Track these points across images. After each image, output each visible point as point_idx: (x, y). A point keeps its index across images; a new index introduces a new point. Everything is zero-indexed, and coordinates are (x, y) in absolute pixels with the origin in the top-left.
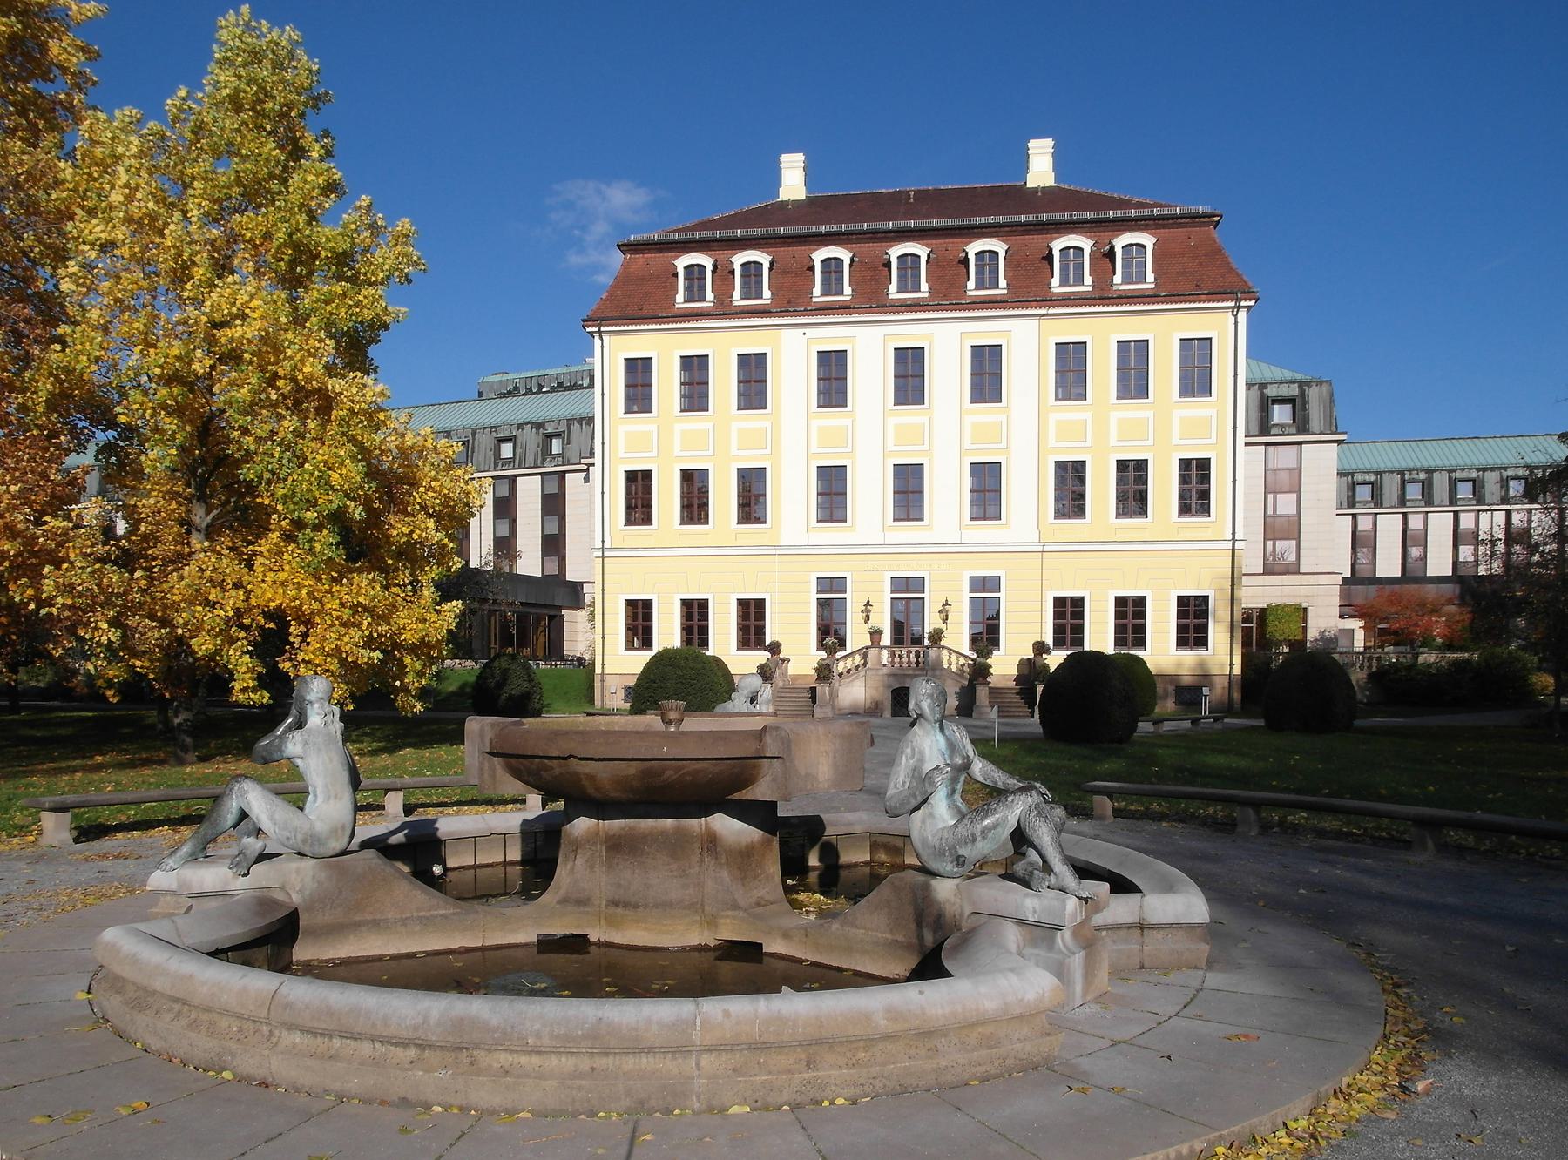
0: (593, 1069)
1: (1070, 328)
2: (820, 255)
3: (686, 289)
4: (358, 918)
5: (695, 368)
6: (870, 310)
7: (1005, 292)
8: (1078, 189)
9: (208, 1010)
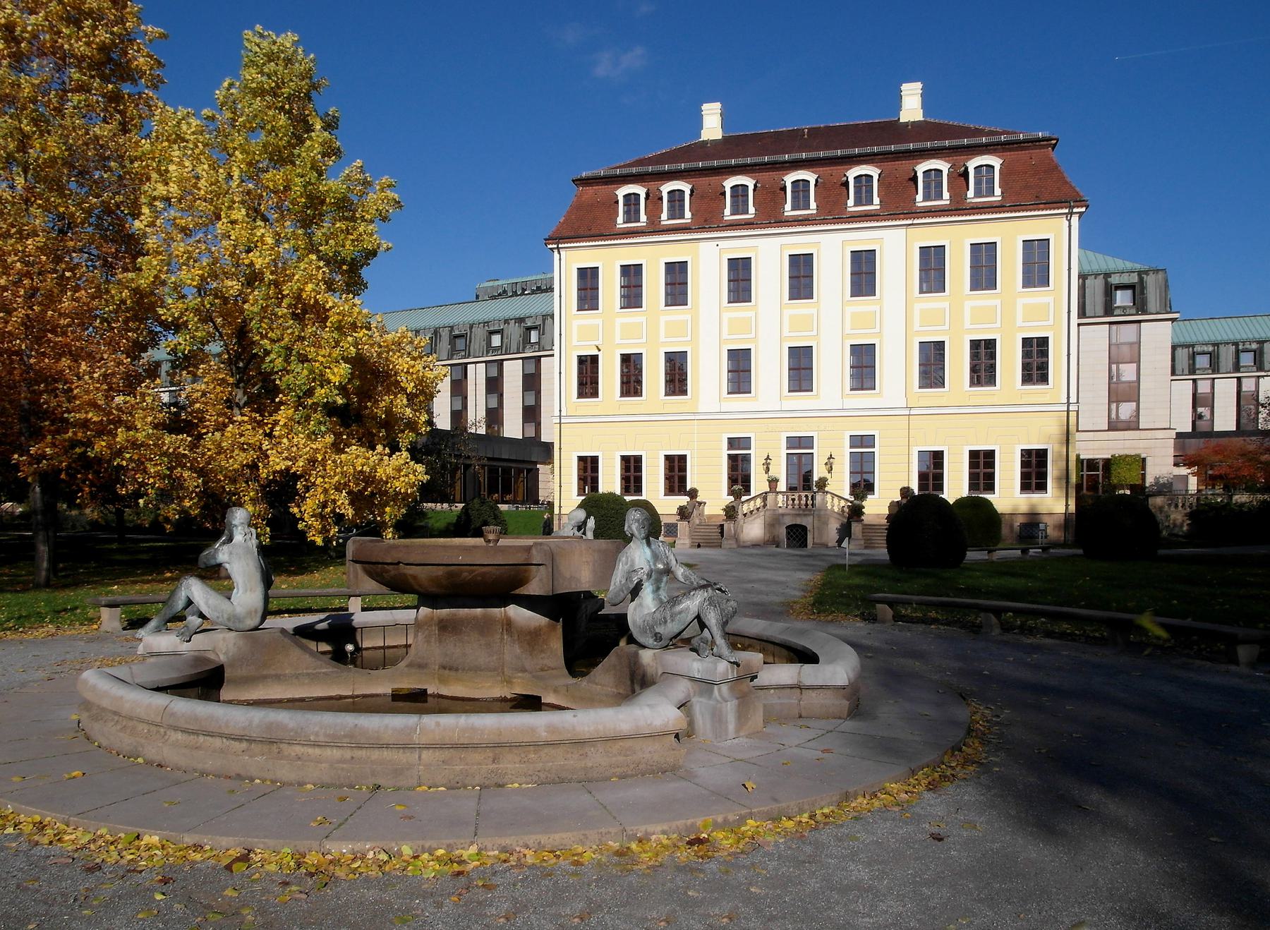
0: (352, 758)
1: (931, 234)
2: (730, 183)
3: (625, 213)
4: (265, 673)
5: (632, 274)
6: (769, 225)
7: (878, 207)
8: (941, 122)
9: (131, 719)
